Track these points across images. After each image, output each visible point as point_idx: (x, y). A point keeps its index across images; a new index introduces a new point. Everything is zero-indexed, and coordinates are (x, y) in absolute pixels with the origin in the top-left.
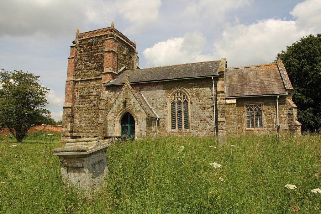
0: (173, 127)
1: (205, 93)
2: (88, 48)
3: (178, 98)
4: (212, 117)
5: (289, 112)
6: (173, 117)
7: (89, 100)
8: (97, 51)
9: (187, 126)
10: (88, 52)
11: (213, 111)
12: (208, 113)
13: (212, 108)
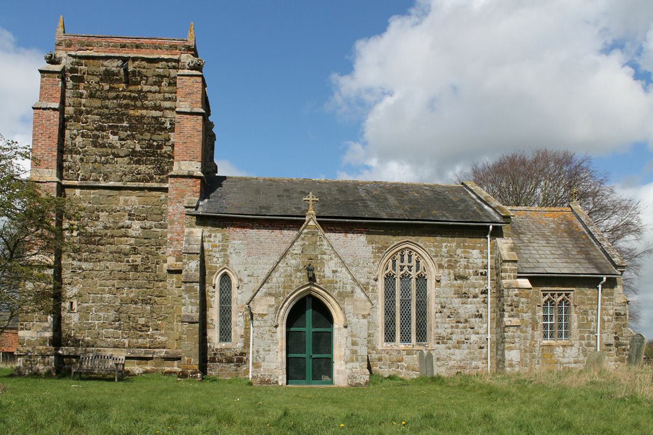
0: (390, 337)
1: (468, 262)
2: (107, 87)
3: (402, 268)
4: (481, 315)
5: (617, 312)
6: (389, 313)
7: (113, 248)
8: (139, 103)
9: (422, 336)
10: (107, 102)
11: (485, 302)
12: (474, 306)
13: (484, 295)
